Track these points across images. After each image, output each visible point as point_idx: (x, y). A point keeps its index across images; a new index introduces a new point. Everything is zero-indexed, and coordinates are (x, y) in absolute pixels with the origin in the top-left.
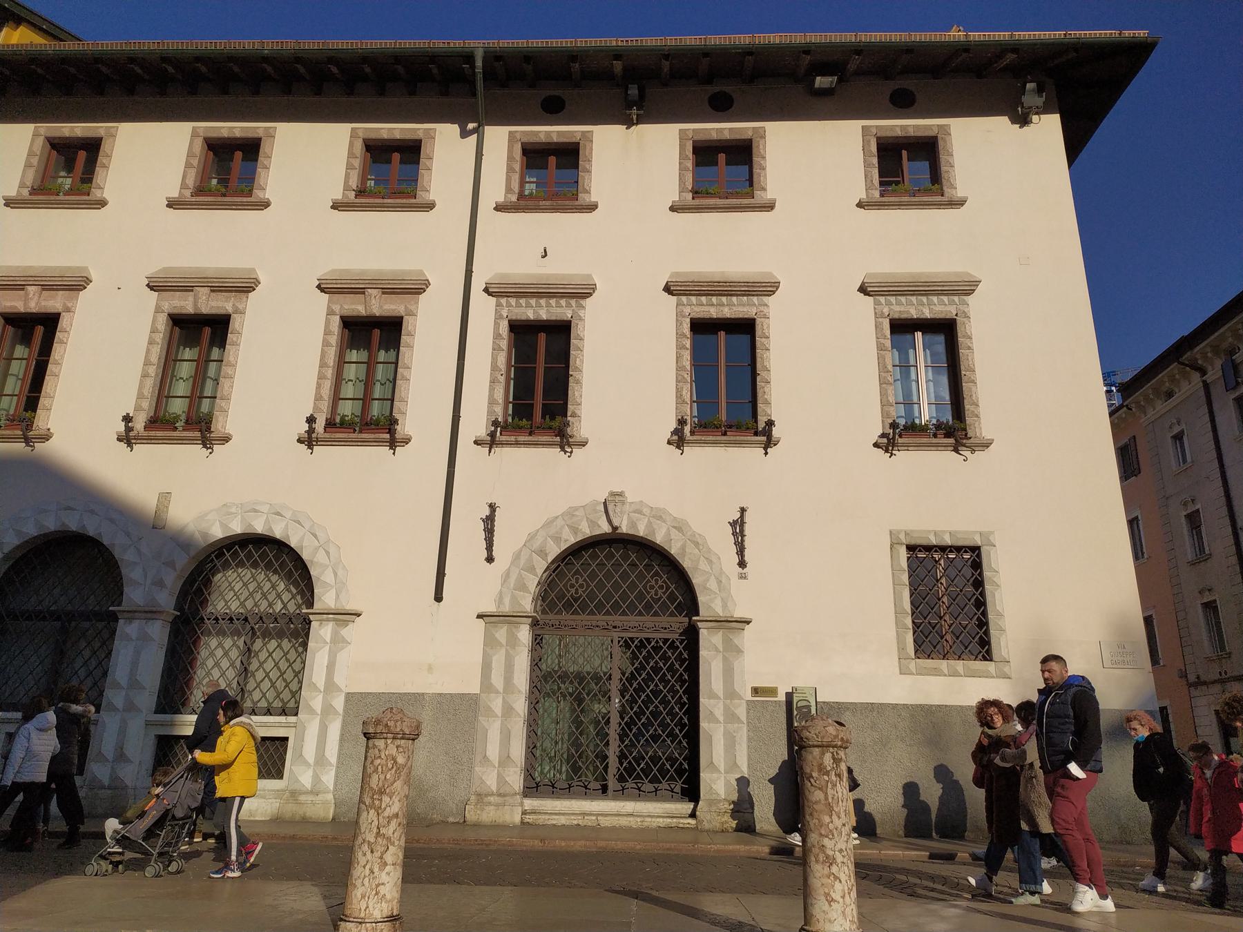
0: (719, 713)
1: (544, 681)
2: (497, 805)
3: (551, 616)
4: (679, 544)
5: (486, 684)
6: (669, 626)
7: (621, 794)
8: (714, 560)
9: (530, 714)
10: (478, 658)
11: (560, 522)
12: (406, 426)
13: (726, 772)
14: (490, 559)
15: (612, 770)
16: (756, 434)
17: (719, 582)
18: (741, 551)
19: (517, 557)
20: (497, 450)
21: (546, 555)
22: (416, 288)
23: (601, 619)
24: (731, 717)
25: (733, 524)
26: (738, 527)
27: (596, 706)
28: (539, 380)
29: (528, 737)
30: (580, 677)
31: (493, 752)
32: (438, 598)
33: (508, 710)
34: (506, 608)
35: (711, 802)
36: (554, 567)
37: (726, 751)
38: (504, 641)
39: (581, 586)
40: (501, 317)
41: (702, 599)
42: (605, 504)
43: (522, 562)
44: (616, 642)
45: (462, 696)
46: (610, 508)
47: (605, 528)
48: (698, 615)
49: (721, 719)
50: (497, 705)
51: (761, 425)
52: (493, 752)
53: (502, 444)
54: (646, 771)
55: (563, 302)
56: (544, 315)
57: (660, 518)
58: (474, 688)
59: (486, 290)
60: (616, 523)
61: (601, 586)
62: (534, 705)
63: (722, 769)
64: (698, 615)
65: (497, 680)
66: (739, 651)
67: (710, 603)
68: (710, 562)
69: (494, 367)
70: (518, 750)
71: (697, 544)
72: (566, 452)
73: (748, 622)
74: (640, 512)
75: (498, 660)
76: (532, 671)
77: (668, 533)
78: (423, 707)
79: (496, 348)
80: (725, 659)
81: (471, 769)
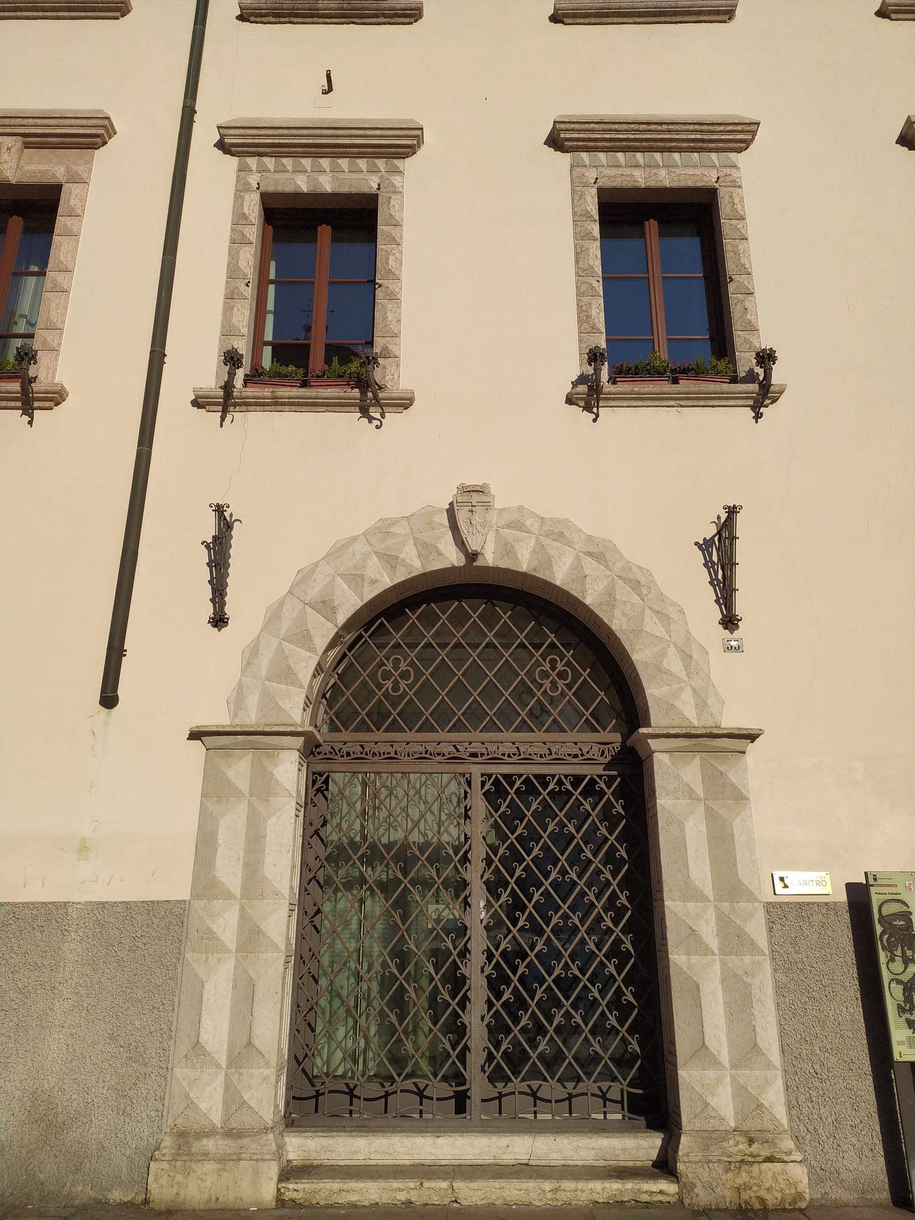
0: (708, 931)
1: (328, 864)
2: (222, 1159)
3: (345, 735)
4: (601, 586)
5: (205, 883)
6: (578, 750)
7: (503, 1121)
8: (674, 616)
9: (301, 937)
10: (191, 825)
11: (361, 547)
12: (56, 368)
13: (734, 1066)
14: (219, 621)
15: (476, 1058)
16: (734, 380)
17: (687, 658)
18: (725, 592)
19: (274, 615)
20: (237, 417)
21: (334, 610)
22: (90, 135)
23: (444, 740)
24: (734, 939)
25: (705, 546)
26: (720, 550)
27: (432, 908)
28: (319, 289)
29: (297, 988)
30: (403, 856)
31: (216, 1032)
32: (109, 699)
33: (251, 937)
34: (251, 718)
35: (710, 1138)
36: (349, 638)
37: (731, 1018)
38: (244, 785)
39: (405, 675)
40: (247, 188)
41: (654, 691)
42: (451, 513)
43: (285, 625)
44: (477, 781)
45: (150, 907)
46: (462, 516)
47: (453, 557)
48: (648, 724)
49: (714, 944)
50: (226, 925)
51: (746, 361)
52: (216, 1032)
53: (247, 405)
54: (552, 1062)
55: (362, 163)
56: (327, 184)
57: (560, 537)
58: (178, 889)
59: (221, 145)
60: (473, 545)
61: (442, 673)
62: (310, 917)
63: (725, 1057)
64: (648, 724)
65: (228, 870)
66: (740, 798)
67: (669, 699)
68: (664, 618)
69: (233, 272)
70: (272, 1027)
71: (636, 586)
72: (371, 419)
73: (752, 737)
74: (519, 526)
75: (232, 826)
76: (306, 846)
77: (577, 565)
78: (64, 932)
79: (238, 240)
80: (711, 816)
81: (166, 1073)
